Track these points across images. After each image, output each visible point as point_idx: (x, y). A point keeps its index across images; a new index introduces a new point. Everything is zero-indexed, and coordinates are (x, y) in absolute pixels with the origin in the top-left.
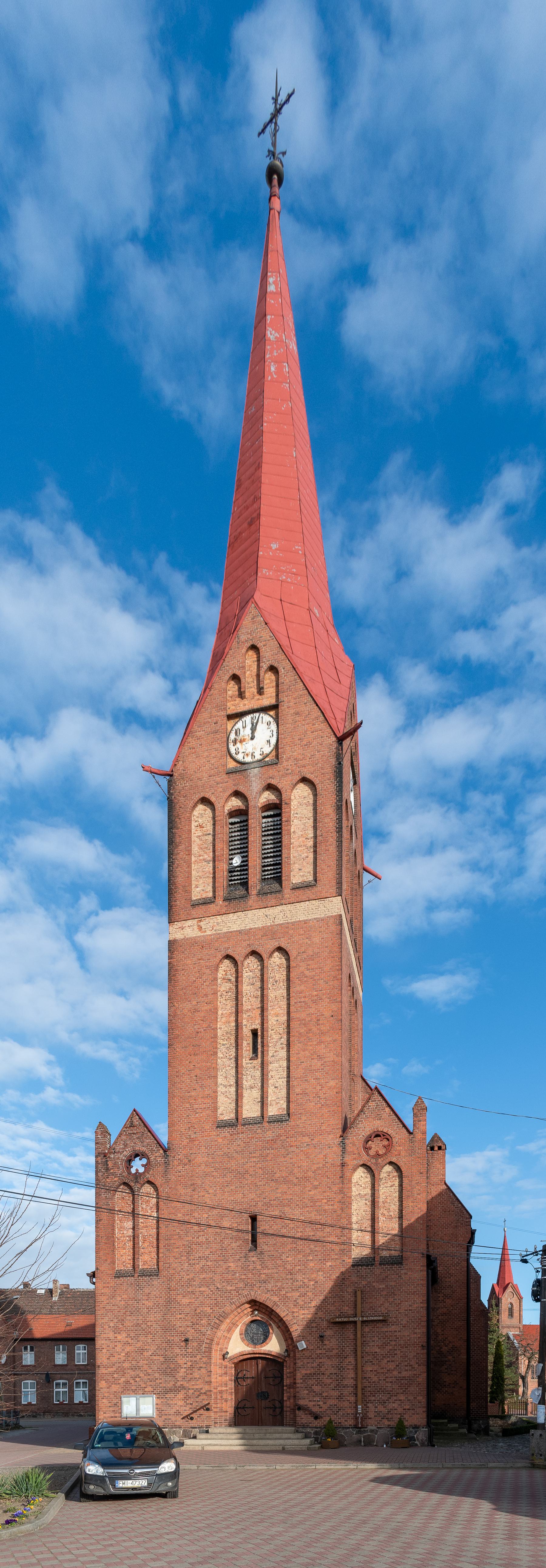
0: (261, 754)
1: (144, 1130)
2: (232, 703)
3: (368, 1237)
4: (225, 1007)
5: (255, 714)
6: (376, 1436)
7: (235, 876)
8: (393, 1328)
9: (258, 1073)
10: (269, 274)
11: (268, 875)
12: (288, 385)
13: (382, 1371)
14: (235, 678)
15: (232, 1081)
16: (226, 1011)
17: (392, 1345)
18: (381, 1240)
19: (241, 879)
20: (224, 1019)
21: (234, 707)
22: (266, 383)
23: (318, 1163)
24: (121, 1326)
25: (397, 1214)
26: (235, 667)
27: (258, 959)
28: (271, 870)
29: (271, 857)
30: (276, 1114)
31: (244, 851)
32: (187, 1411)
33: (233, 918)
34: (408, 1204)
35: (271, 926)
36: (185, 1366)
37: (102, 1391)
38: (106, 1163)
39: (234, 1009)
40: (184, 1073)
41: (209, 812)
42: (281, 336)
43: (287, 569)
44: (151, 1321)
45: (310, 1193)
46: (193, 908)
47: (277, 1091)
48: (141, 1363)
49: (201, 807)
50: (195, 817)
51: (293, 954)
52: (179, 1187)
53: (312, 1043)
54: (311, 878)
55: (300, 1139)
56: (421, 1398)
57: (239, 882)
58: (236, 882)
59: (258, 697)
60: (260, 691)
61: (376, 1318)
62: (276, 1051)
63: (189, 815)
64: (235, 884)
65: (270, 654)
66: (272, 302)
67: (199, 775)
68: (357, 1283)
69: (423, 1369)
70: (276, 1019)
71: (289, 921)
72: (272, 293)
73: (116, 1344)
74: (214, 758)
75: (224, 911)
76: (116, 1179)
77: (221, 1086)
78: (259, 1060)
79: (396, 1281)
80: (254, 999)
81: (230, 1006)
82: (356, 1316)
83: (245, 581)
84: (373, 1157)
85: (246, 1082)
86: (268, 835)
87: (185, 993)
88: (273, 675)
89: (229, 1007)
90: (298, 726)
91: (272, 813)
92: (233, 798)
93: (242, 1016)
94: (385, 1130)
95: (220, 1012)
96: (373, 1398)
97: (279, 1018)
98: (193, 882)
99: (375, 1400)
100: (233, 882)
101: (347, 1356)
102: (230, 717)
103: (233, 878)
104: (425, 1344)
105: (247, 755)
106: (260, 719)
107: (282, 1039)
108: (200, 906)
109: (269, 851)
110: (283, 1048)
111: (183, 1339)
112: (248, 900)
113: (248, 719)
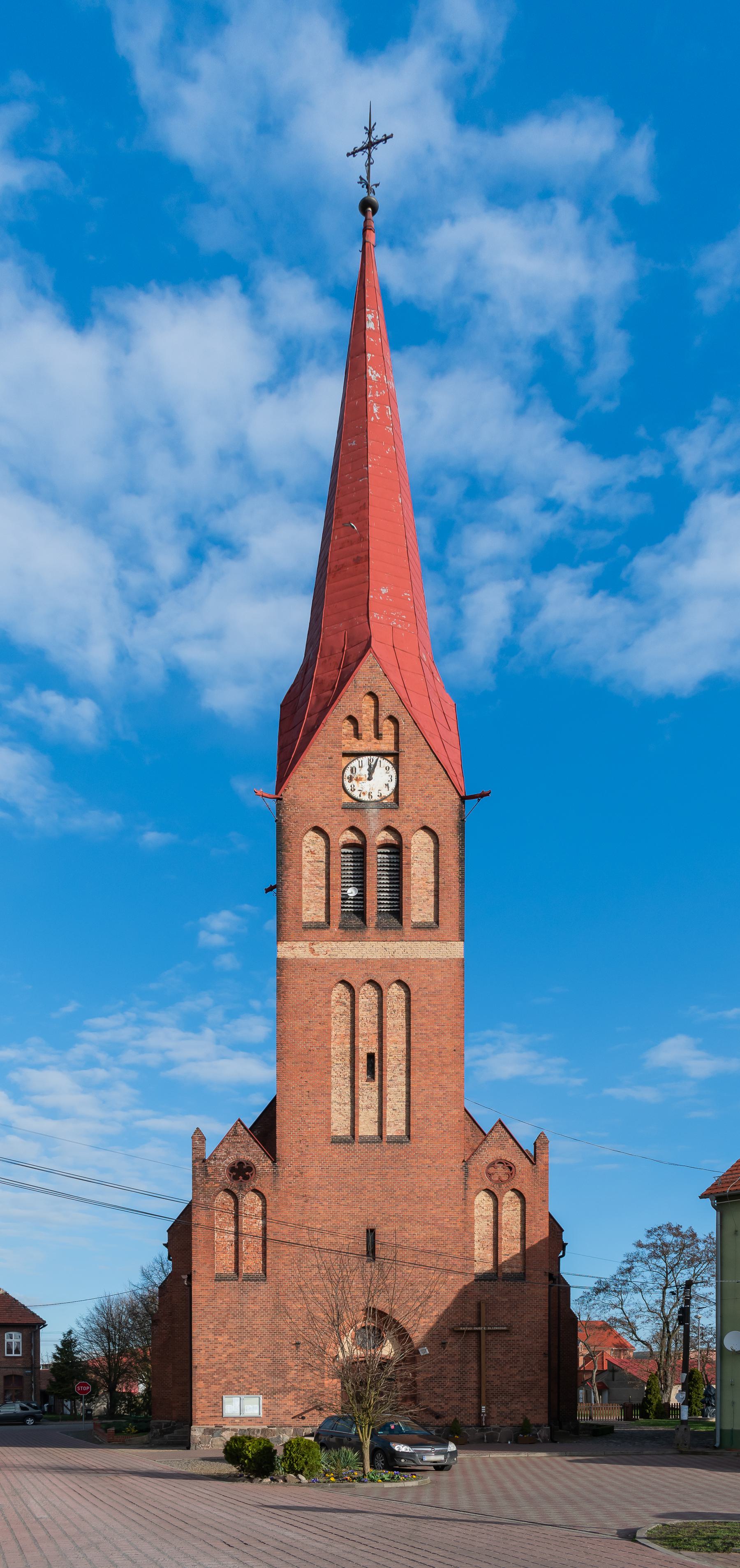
0: (378, 796)
1: (250, 1140)
2: (347, 741)
3: (490, 1255)
4: (339, 1028)
5: (372, 757)
6: (499, 1434)
7: (347, 904)
8: (516, 1337)
9: (375, 1095)
10: (367, 310)
11: (383, 908)
12: (391, 429)
13: (505, 1375)
14: (352, 719)
15: (348, 1100)
16: (340, 1033)
17: (514, 1353)
18: (503, 1258)
19: (354, 908)
20: (337, 1040)
21: (349, 745)
22: (369, 423)
23: (439, 1185)
24: (222, 1328)
25: (519, 1235)
26: (351, 709)
27: (375, 987)
28: (387, 904)
29: (387, 892)
30: (394, 1134)
31: (360, 881)
32: (298, 1410)
33: (349, 946)
34: (531, 1229)
35: (390, 959)
36: (296, 1368)
37: (199, 1390)
38: (205, 1169)
39: (349, 1032)
40: (295, 1088)
41: (321, 840)
42: (382, 377)
43: (397, 615)
44: (257, 1325)
45: (432, 1212)
46: (305, 930)
47: (396, 1114)
48: (245, 1365)
49: (312, 834)
50: (305, 842)
51: (414, 989)
52: (289, 1198)
53: (433, 1073)
54: (431, 919)
55: (421, 1160)
56: (544, 1400)
57: (352, 910)
58: (349, 910)
59: (376, 741)
60: (378, 736)
61: (500, 1328)
62: (394, 1076)
63: (300, 841)
64: (348, 911)
65: (389, 704)
66: (372, 340)
67: (312, 804)
68: (480, 1296)
69: (546, 1374)
70: (395, 1046)
71: (409, 957)
72: (371, 330)
73: (216, 1345)
74: (328, 791)
75: (339, 938)
76: (216, 1185)
77: (334, 1104)
78: (377, 1082)
79: (519, 1295)
80: (371, 1025)
81: (345, 1029)
82: (479, 1325)
83: (353, 618)
84: (496, 1182)
85: (362, 1102)
86: (384, 870)
87: (296, 1012)
88: (391, 723)
89: (343, 1029)
90: (419, 777)
91: (389, 851)
92: (348, 832)
93: (358, 1040)
94: (508, 1159)
95: (333, 1033)
96: (496, 1400)
97: (397, 1046)
98: (303, 905)
99: (498, 1402)
100: (346, 910)
101: (469, 1361)
102: (345, 755)
103: (346, 906)
104: (547, 1353)
105: (364, 794)
106: (378, 762)
107: (401, 1066)
108: (313, 930)
109: (385, 886)
110: (401, 1074)
111: (294, 1343)
112: (366, 932)
113: (365, 760)
